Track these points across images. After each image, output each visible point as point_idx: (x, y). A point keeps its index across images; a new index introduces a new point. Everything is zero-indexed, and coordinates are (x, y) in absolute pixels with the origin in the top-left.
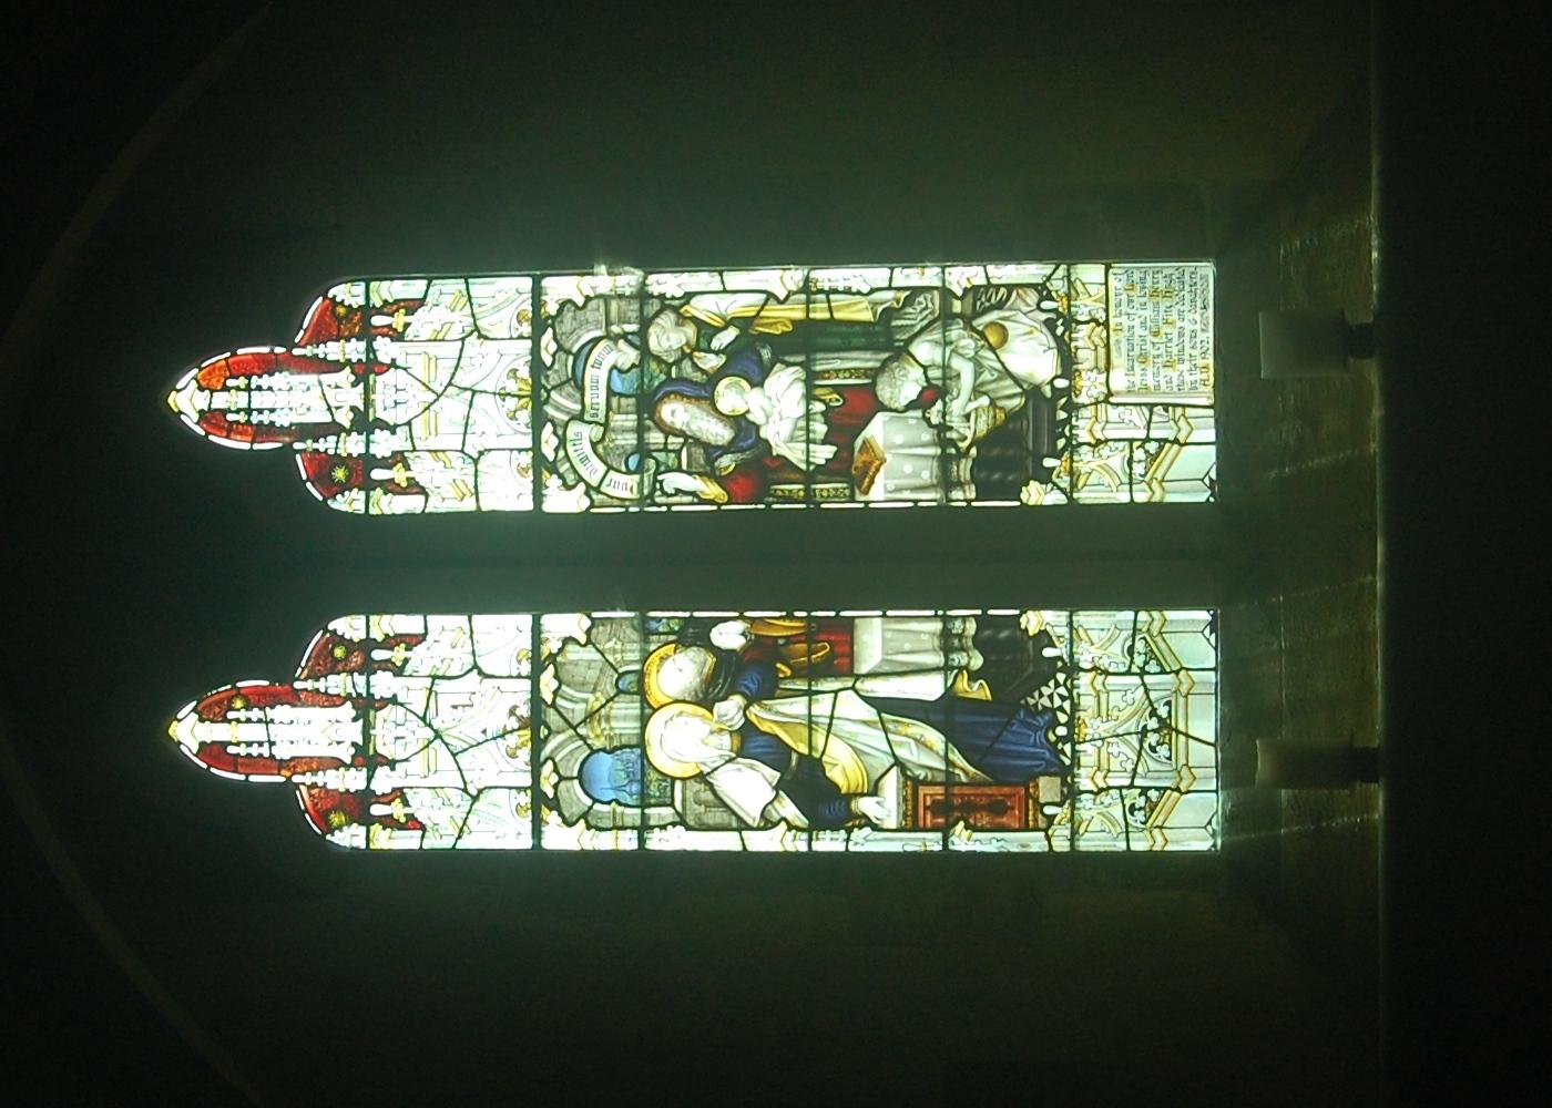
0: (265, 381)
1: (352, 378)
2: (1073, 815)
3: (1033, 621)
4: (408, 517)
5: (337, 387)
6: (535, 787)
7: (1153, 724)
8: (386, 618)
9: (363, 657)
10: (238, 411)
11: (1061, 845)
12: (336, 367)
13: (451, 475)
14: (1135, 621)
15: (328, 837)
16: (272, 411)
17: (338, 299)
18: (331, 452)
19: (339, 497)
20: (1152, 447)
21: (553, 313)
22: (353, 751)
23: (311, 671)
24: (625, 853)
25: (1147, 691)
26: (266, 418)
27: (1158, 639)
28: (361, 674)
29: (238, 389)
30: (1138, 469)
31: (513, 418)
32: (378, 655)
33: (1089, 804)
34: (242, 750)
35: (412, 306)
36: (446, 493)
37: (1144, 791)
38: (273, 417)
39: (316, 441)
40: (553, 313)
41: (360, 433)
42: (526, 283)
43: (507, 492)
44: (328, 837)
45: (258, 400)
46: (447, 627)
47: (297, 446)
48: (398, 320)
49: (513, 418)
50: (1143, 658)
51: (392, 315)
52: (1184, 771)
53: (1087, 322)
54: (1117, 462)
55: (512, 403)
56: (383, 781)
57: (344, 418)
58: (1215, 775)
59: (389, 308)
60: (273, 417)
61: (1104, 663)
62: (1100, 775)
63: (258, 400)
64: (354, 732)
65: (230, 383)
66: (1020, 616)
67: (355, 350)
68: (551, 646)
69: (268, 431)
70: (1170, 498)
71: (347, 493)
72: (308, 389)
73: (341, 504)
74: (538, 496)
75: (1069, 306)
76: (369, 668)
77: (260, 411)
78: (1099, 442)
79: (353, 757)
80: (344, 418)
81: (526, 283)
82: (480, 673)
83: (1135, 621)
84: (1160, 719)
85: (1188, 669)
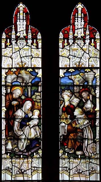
0: (83, 20)
1: (25, 36)
2: (8, 158)
3: (40, 151)
4: (58, 46)
5: (81, 33)
6: (12, 68)
7: (81, 171)
8: (99, 41)
9: (92, 37)
10: (78, 15)
11: (3, 156)
12: (27, 33)
13: (8, 53)
14: (40, 168)
15: (61, 32)
16: (77, 22)
17: (97, 33)
18: (29, 32)
19: (62, 33)
20: (11, 171)
21: (93, 71)
22: (18, 36)
23: (90, 28)
24: (2, 82)
25: (28, 170)
26: (76, 21)
27: (37, 172)
28: (89, 37)
29: (82, 15)
30: (65, 169)
31: (18, 64)
32: (93, 40)
33: (10, 160)
34: (18, 16)
35: (95, 47)
36: (63, 52)
37: (12, 169)
38: (76, 22)
39: (14, 29)
40: (93, 71)
41: (73, 37)
42: (98, 66)
43: (63, 62)
44: (61, 32)
45: (79, 19)
46: (39, 52)
47: (71, 26)
48: (93, 44)
49: (18, 64)
50: (34, 169)
51: (36, 43)
52: (73, 176)
53: (32, 160)
54: (66, 165)
55: (78, 64)
56: (14, 42)
57: (18, 34)
58: (65, 179)
59: (95, 43)
60: (76, 22)
61: (33, 163)
62: (14, 162)
63: (79, 19)
64: (22, 36)
65: (83, 14)
66: (41, 149)
67: (30, 36)
68: (36, 71)
69: (16, 21)
70: (60, 174)
71: (5, 34)
72: (23, 28)
73: (61, 34)
74: (62, 68)
75: (34, 158)
76: (90, 39)
77: (77, 19)
78: (70, 162)
79: (75, 36)
80: (18, 34)
81: (40, 66)
82: (89, 58)
83: (40, 168)
84: (24, 172)
85: (90, 177)
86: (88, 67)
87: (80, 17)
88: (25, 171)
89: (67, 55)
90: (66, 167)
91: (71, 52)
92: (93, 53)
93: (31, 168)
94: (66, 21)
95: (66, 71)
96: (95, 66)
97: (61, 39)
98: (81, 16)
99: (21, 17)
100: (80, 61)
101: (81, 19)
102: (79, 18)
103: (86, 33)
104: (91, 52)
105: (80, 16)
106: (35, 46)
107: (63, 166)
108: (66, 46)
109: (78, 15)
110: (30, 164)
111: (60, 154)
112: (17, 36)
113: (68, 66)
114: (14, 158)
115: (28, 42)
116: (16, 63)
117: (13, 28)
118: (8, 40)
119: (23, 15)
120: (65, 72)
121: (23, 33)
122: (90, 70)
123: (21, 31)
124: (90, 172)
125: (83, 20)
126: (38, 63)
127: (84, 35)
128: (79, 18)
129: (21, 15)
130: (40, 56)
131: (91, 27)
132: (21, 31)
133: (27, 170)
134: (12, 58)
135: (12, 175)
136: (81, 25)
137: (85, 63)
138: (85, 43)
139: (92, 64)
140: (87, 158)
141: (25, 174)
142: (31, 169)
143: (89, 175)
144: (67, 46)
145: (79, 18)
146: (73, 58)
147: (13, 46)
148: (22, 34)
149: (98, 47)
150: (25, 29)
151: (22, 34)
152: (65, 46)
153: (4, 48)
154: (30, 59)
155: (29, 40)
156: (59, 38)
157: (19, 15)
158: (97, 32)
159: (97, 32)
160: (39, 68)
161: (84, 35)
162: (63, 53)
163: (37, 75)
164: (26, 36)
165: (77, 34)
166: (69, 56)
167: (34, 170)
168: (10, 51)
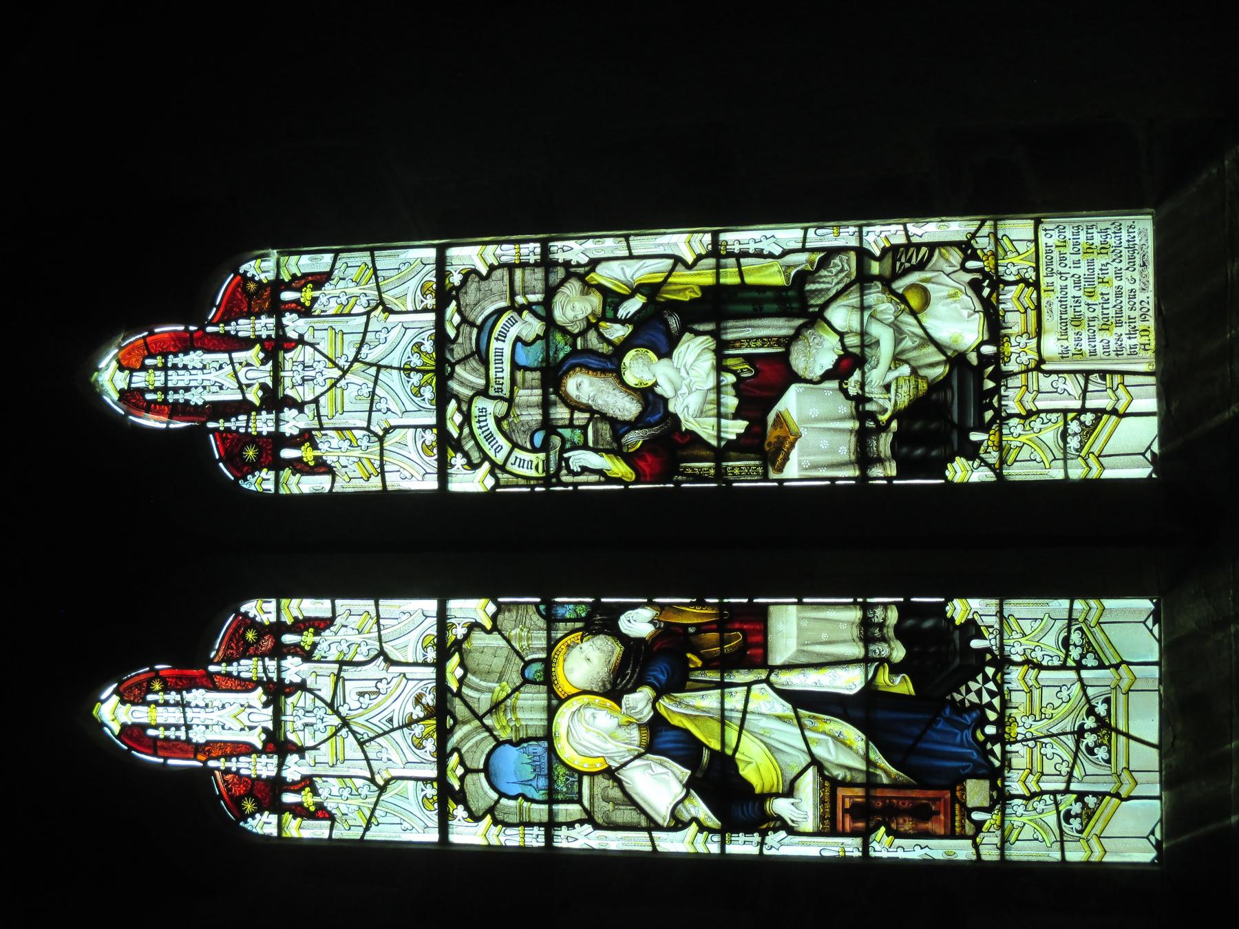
0: (181, 360)
1: (262, 355)
3: (959, 610)
7: (1090, 723)
8: (295, 602)
10: (155, 391)
11: (990, 854)
12: (246, 344)
14: (1071, 610)
16: (187, 389)
18: (242, 430)
22: (263, 737)
23: (223, 315)
25: (1084, 687)
26: (181, 397)
27: (1096, 630)
28: (272, 659)
30: (1074, 443)
33: (1020, 810)
34: (161, 733)
35: (320, 280)
38: (188, 396)
41: (269, 412)
43: (412, 472)
45: (175, 379)
47: (211, 425)
49: (418, 394)
50: (1079, 650)
54: (1050, 435)
55: (415, 378)
57: (254, 396)
60: (188, 396)
61: (1037, 656)
63: (175, 379)
65: (148, 362)
66: (945, 604)
67: (264, 326)
76: (280, 652)
77: (176, 390)
80: (254, 396)
86: (432, 669)
87: (163, 378)
88: (1091, 711)
89: (364, 443)
90: (1064, 435)
91: (351, 424)
92: (357, 639)
93: (1070, 668)
94: (190, 468)
95: (459, 455)
96: (430, 627)
97: (280, 826)
98: (158, 373)
99: (173, 715)
100: (399, 369)
101: (175, 367)
102: (170, 384)
103: (250, 680)
104: (352, 301)
105: (158, 379)
106: (316, 294)
107: (1059, 455)
108: (317, 453)
109: (155, 391)
110: (1044, 674)
111: (982, 475)
112: (265, 743)
113: (431, 791)
114: (1000, 400)
115: (297, 680)
116: (410, 407)
117: (221, 425)
118: (287, 453)
119: (156, 703)
120: (465, 814)
121: (248, 365)
122: (454, 303)
123: (239, 382)
124: (1095, 663)
125: (176, 355)
126: (409, 619)
127: (260, 690)
128: (166, 380)
129: (158, 715)
130: (369, 604)
131: (218, 307)
132: (239, 382)
133: (1085, 694)
134: (386, 431)
135: (1114, 412)
136: (204, 367)
137: (408, 691)
138: (302, 686)
139: (419, 292)
140: (1002, 678)
141: (1109, 711)
142: (1083, 410)
143: (1117, 667)
144: (315, 792)
145: (170, 384)
146: (383, 406)
147: (319, 770)
148: (251, 375)
149: (322, 262)
150: (224, 357)
151: (251, 375)
152: (315, 804)
153: (333, 481)
154: (393, 318)
155: (283, 675)
156: (275, 834)
157: (156, 727)
158: (246, 272)
159: (246, 272)
160: (441, 262)
161: (260, 690)
162: (355, 467)
163: (475, 271)
164: (262, 350)
165: (251, 728)
166: (376, 435)
167: (1088, 647)
168: (346, 793)
